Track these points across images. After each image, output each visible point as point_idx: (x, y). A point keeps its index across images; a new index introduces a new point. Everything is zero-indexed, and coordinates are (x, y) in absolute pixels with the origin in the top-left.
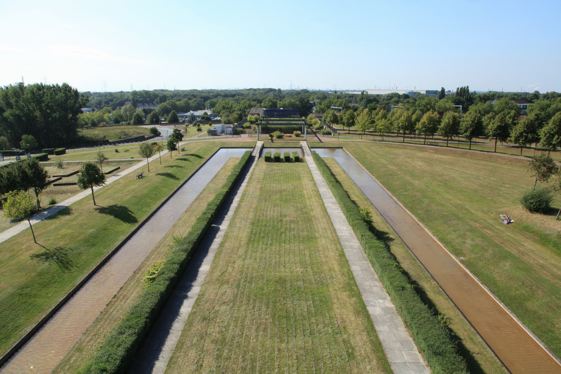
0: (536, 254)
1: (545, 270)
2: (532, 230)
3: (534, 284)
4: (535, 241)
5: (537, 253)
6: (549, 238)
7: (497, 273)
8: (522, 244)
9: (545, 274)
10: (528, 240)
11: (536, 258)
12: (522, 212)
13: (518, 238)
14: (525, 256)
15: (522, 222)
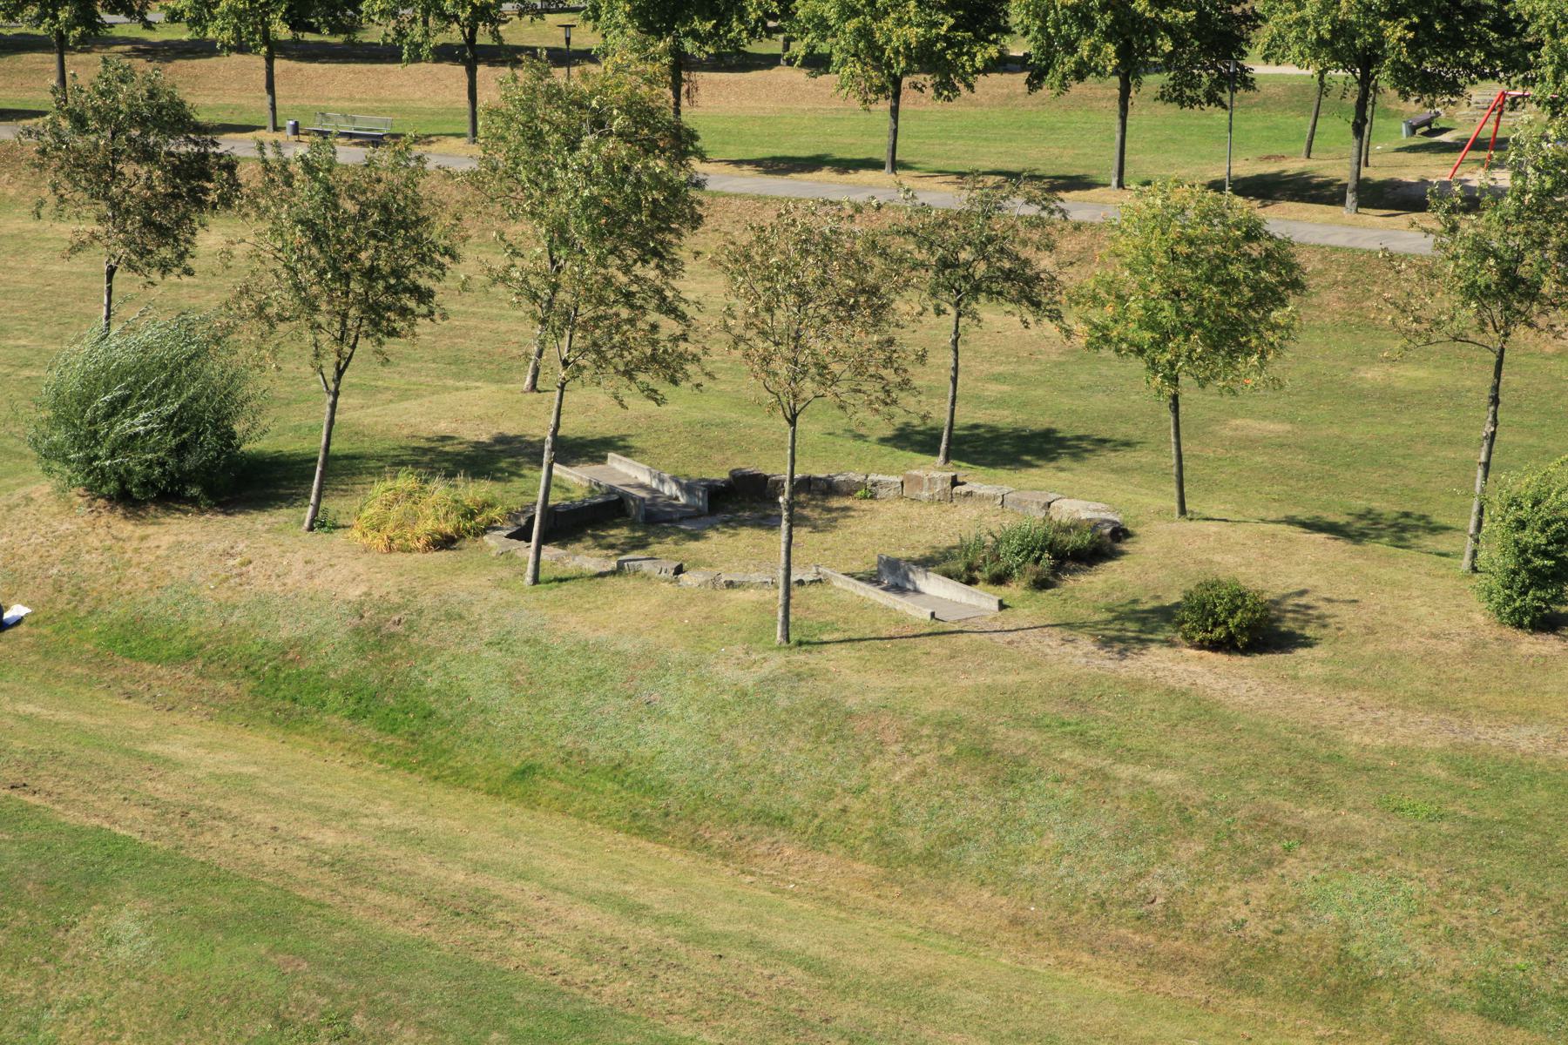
0: (275, 800)
1: (373, 886)
2: (179, 644)
3: (353, 996)
4: (223, 710)
5: (276, 791)
6: (310, 665)
7: (71, 1007)
8: (155, 756)
9: (379, 910)
10: (177, 717)
11: (282, 825)
12: (65, 527)
13: (102, 722)
14: (216, 832)
15: (89, 602)
